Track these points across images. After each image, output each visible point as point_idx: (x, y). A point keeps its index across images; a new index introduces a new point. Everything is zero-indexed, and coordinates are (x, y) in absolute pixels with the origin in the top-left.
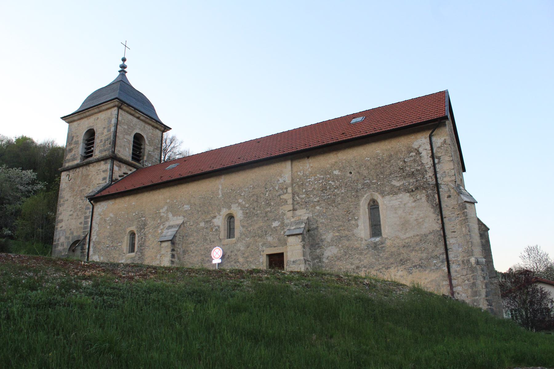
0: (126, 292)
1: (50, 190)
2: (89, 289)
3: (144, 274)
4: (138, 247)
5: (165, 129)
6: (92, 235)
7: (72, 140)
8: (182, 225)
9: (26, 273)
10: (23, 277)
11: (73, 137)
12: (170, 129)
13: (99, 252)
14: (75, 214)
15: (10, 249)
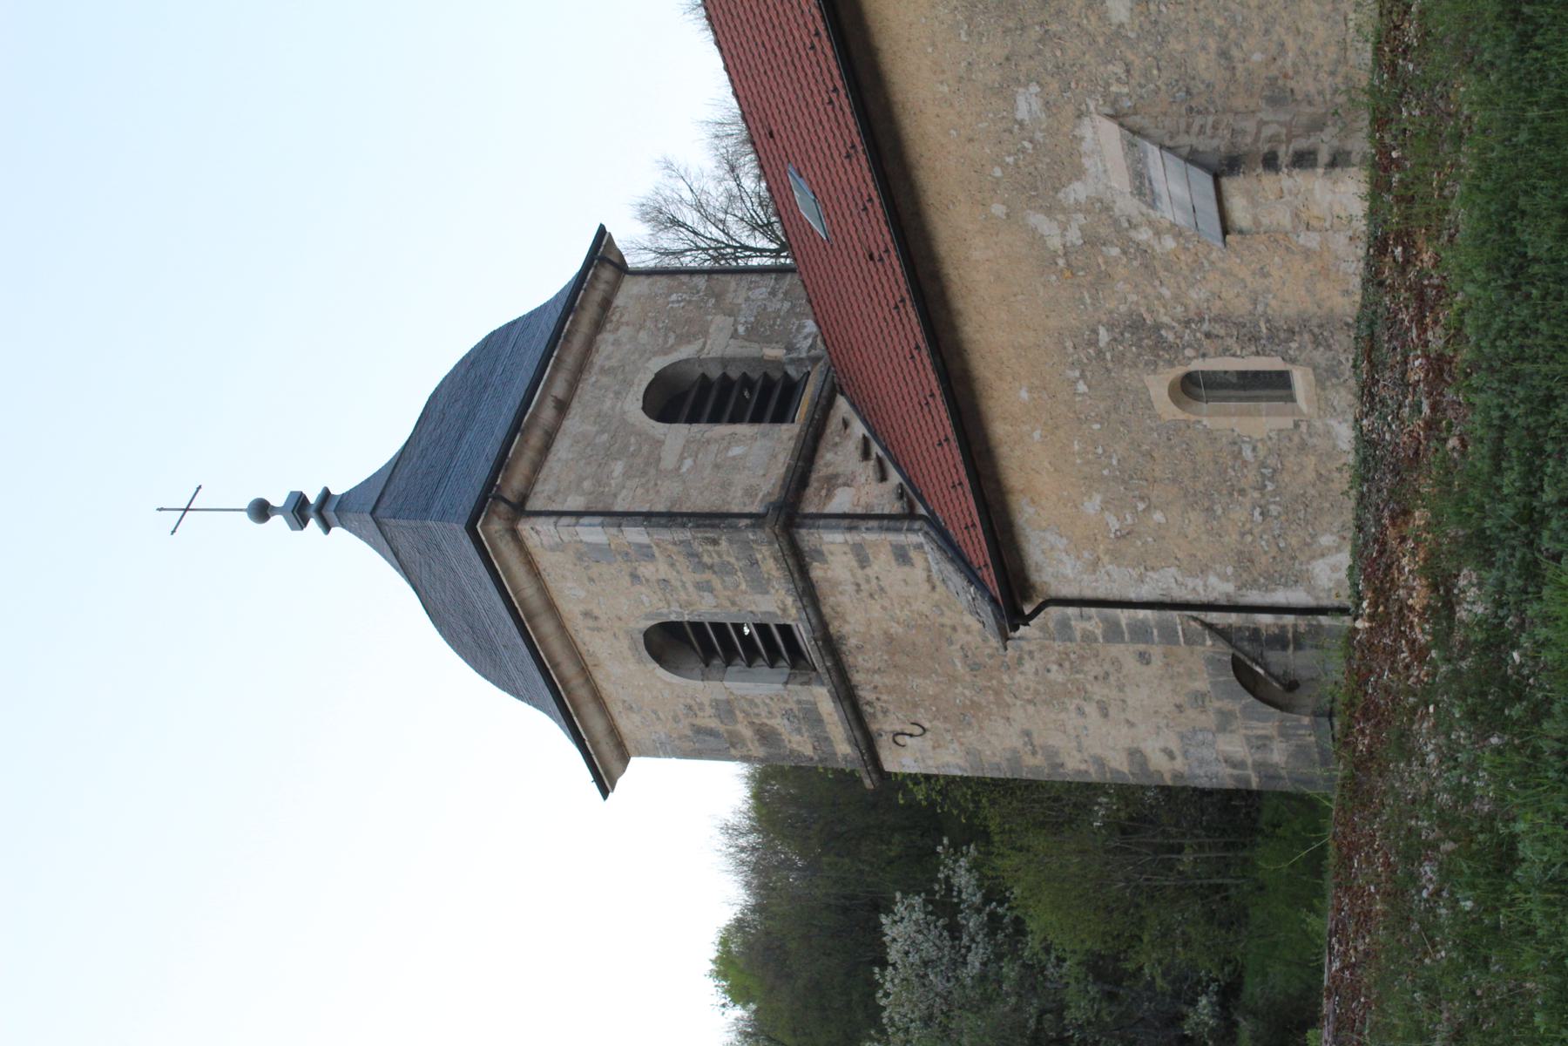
0: (1517, 388)
1: (977, 822)
2: (1503, 584)
3: (1413, 304)
4: (1257, 354)
5: (604, 260)
6: (1203, 596)
7: (712, 733)
8: (1130, 121)
9: (1425, 894)
10: (1443, 911)
11: (699, 730)
12: (602, 231)
13: (1294, 558)
14: (1098, 691)
15: (1291, 991)
